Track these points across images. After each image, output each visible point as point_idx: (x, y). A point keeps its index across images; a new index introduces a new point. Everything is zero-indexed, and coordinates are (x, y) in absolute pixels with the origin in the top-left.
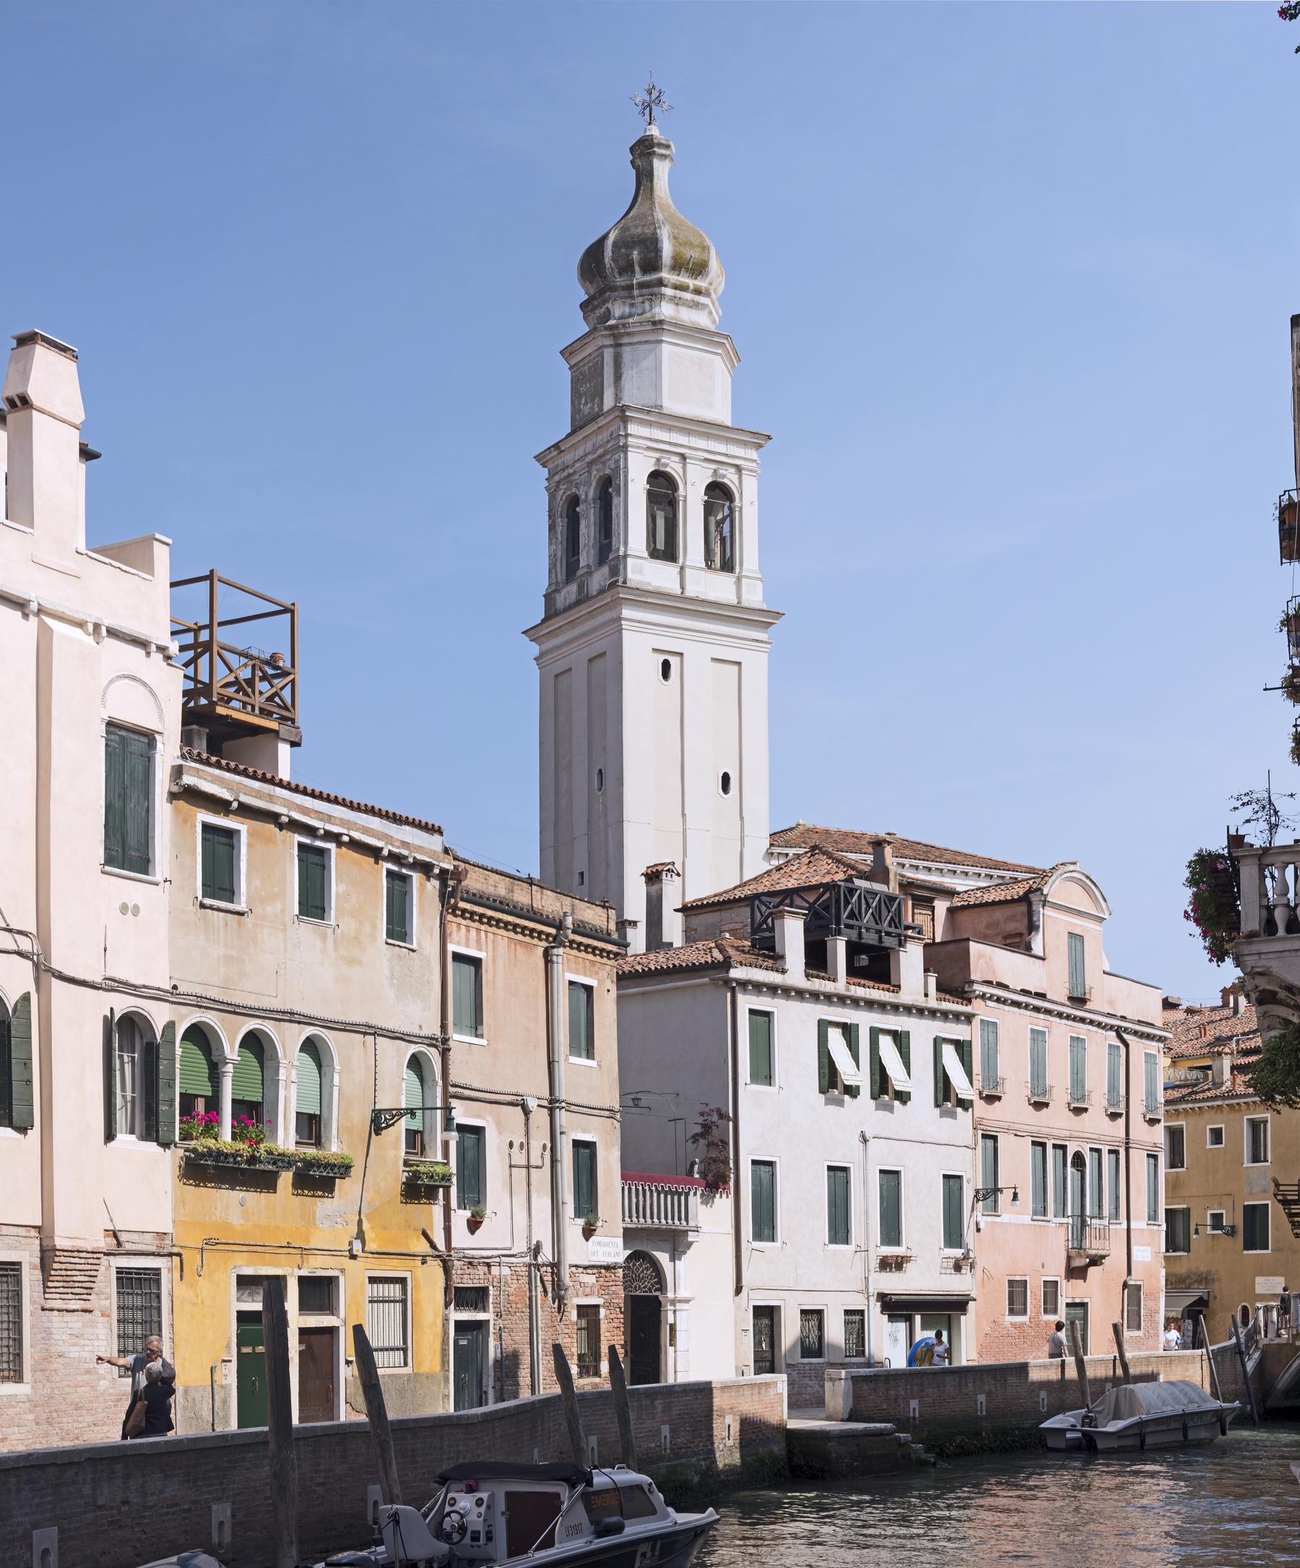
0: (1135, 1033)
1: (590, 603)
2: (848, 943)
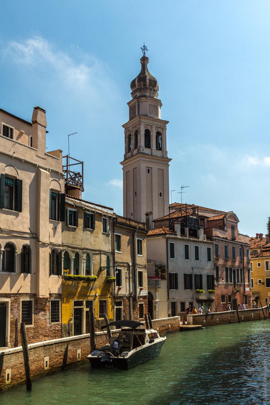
0: (245, 245)
1: (133, 157)
2: (189, 229)
